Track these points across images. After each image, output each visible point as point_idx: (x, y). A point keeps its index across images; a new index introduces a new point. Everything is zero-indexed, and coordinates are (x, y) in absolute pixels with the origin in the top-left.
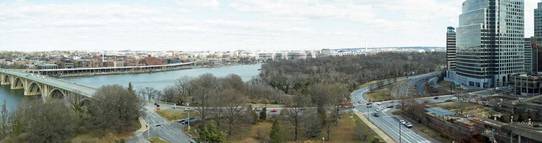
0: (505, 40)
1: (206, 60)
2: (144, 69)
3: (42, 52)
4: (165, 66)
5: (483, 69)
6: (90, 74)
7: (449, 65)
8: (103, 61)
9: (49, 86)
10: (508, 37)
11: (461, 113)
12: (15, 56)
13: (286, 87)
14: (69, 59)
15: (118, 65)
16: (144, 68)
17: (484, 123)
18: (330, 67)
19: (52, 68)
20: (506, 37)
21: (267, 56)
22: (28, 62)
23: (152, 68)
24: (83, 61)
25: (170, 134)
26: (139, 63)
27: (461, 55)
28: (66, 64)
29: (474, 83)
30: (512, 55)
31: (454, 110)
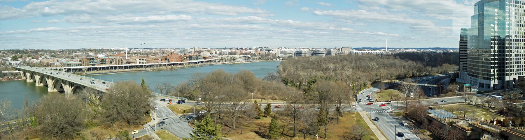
0: (515, 41)
1: (227, 57)
2: (166, 66)
3: (69, 50)
4: (187, 63)
5: (493, 70)
6: (113, 71)
7: (461, 66)
8: (127, 58)
9: (70, 83)
10: (519, 39)
11: (464, 116)
12: (41, 54)
13: (299, 84)
14: (94, 56)
15: (141, 62)
16: (166, 64)
17: (483, 127)
18: (347, 65)
19: (77, 66)
20: (517, 38)
21: (288, 53)
22: (53, 60)
23: (174, 65)
24: (107, 59)
25: (176, 127)
26: (161, 60)
27: (473, 57)
28: (90, 61)
29: (484, 84)
30: (523, 57)
31: (458, 112)
